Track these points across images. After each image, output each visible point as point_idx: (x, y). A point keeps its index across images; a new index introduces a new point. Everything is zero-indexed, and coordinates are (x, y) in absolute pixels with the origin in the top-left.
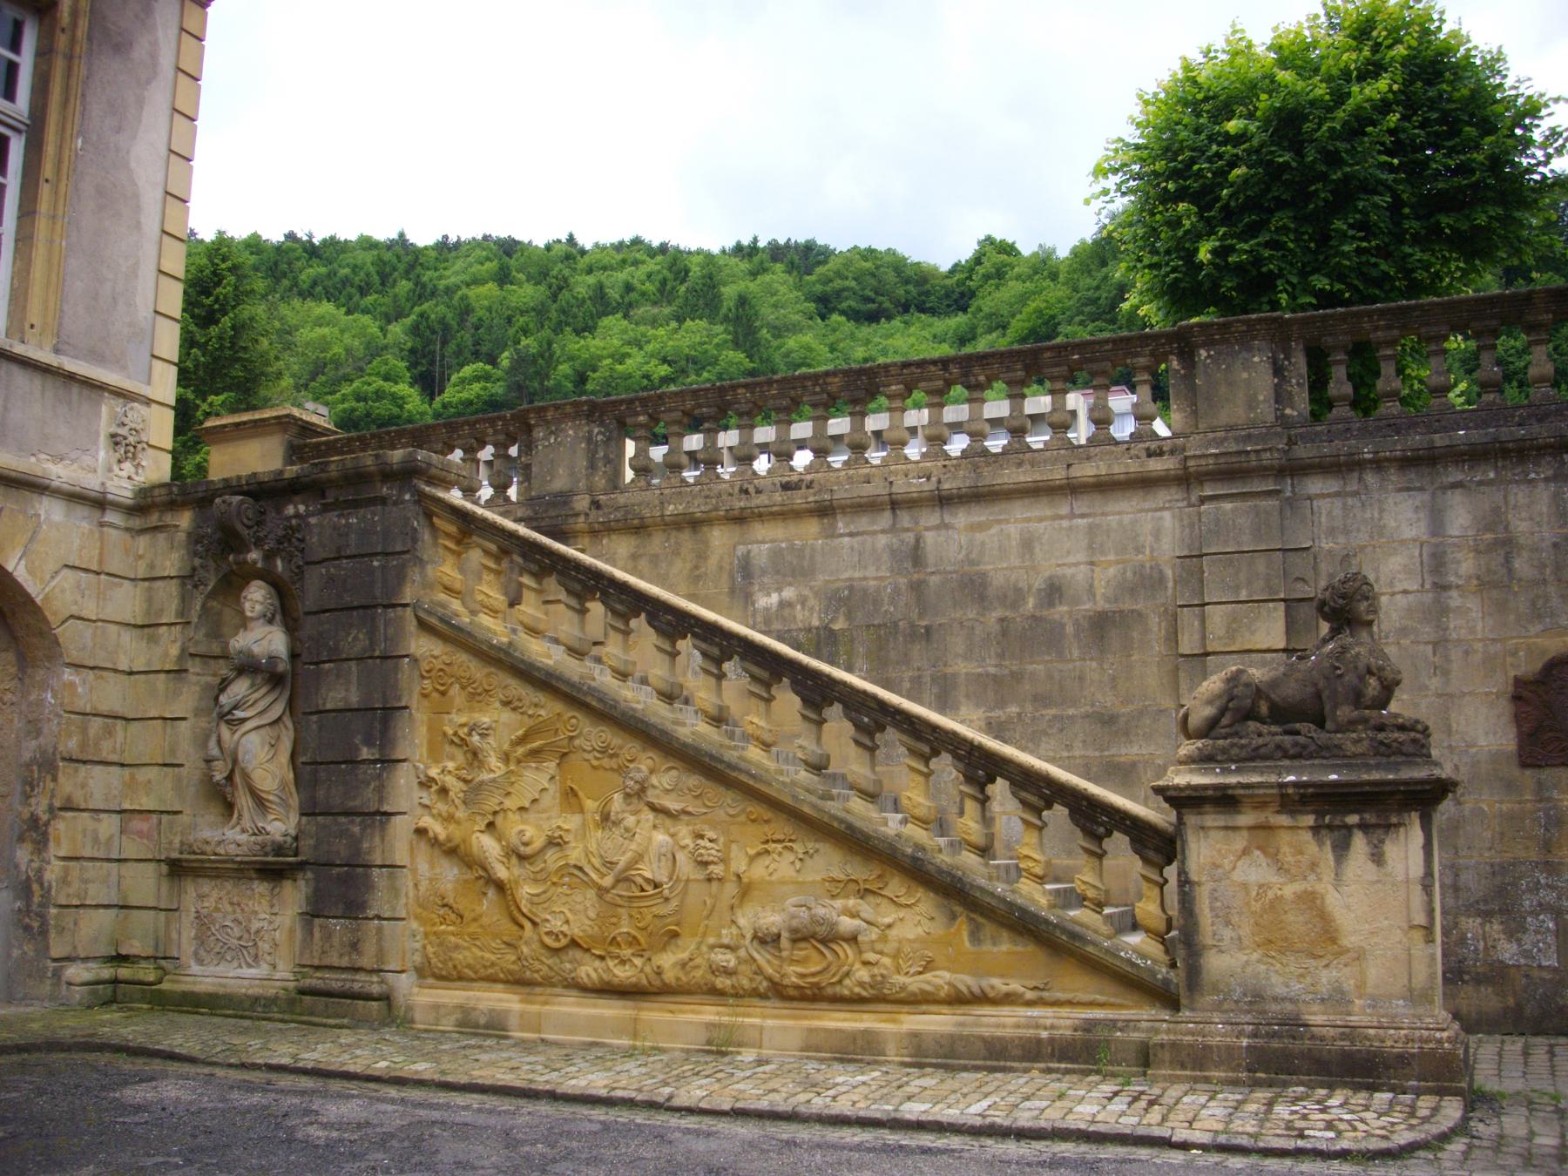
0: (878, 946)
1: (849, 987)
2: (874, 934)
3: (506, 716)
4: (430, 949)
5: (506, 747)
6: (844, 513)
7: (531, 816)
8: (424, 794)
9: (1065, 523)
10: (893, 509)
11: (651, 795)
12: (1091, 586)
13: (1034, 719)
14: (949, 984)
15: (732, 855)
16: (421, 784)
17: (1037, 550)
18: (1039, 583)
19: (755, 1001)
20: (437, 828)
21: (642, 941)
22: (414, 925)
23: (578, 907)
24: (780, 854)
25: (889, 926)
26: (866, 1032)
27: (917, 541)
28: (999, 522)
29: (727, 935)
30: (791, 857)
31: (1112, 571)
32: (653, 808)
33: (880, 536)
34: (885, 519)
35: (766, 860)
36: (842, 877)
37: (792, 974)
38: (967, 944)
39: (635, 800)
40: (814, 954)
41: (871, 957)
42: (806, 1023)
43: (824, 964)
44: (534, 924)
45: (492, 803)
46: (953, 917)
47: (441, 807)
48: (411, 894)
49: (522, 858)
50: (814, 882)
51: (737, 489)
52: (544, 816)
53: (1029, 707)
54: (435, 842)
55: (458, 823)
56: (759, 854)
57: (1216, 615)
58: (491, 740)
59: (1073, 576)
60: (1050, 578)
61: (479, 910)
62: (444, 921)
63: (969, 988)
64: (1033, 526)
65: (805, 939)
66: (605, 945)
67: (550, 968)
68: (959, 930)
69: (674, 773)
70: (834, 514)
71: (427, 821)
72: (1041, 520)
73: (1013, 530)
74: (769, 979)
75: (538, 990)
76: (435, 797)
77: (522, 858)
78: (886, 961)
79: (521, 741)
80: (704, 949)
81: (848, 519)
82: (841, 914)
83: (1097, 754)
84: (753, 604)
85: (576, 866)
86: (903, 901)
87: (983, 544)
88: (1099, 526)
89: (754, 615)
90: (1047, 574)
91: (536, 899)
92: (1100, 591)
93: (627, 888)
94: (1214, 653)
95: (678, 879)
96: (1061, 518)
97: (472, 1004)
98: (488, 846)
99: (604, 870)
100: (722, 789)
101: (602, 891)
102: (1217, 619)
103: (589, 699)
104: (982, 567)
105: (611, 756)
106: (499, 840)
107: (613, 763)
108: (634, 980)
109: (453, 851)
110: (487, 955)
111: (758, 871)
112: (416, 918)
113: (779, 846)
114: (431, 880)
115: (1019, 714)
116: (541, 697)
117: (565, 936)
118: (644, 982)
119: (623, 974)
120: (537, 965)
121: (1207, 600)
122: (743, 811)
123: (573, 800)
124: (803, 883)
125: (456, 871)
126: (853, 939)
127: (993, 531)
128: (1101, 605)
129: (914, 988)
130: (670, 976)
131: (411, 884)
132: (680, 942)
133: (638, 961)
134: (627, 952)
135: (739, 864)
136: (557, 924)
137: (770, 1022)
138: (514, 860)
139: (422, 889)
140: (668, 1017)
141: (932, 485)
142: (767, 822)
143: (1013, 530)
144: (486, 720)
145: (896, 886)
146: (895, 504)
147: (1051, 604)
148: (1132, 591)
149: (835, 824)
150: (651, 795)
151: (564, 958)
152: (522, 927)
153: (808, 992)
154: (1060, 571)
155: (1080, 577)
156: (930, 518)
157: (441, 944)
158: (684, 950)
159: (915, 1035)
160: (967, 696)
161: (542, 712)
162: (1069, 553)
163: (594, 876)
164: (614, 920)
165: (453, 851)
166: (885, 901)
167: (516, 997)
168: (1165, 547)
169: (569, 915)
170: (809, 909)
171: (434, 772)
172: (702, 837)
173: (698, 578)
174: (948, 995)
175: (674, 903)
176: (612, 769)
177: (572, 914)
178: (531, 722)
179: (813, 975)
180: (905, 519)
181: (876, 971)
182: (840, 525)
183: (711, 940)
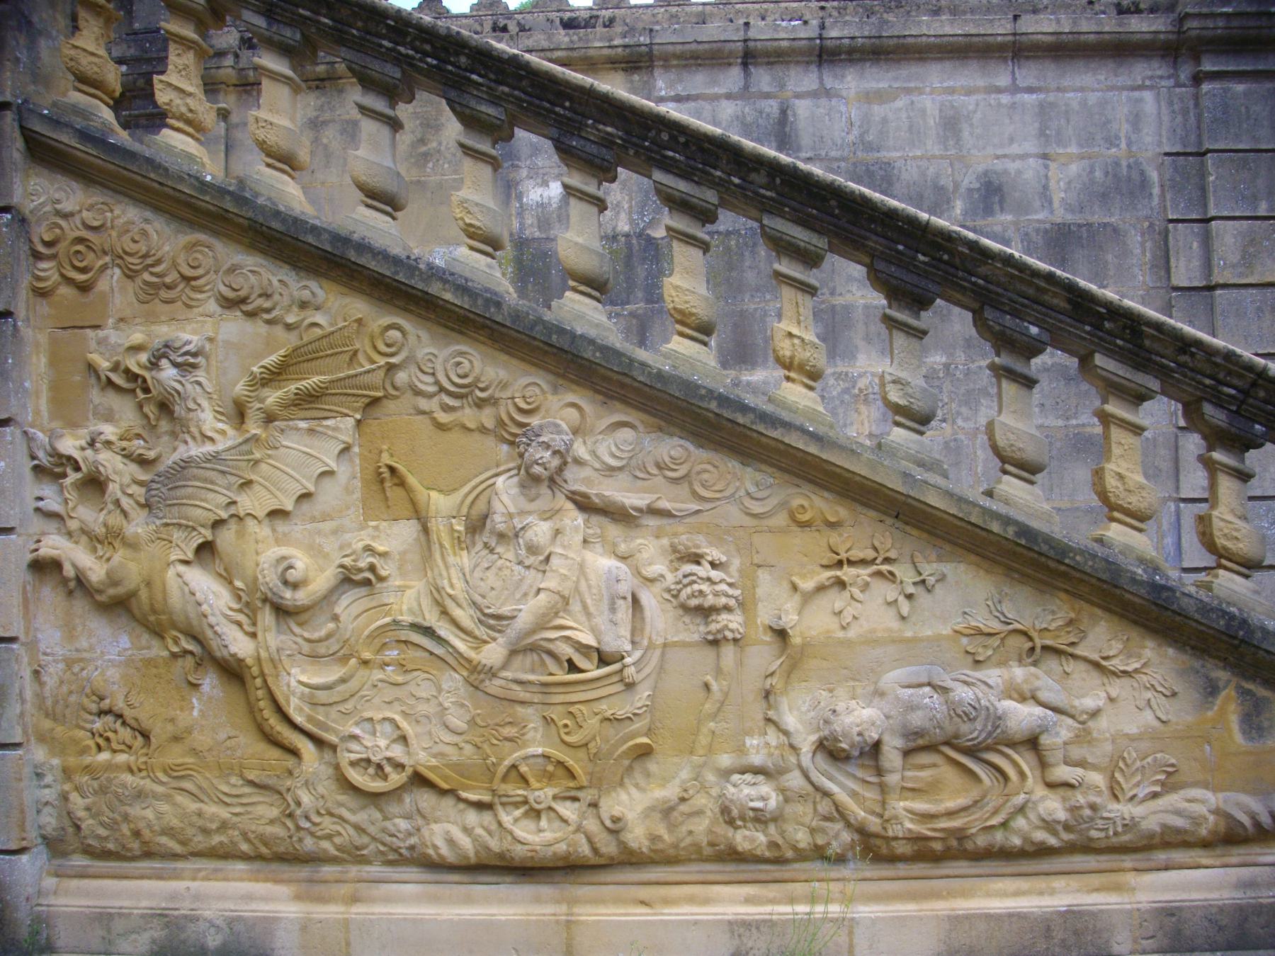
0: (1076, 753)
1: (1025, 829)
2: (1064, 730)
3: (233, 327)
4: (77, 801)
5: (240, 388)
6: (666, 67)
7: (297, 528)
8: (48, 490)
9: (1005, 99)
10: (745, 65)
11: (576, 479)
12: (1046, 187)
13: (968, 373)
14: (1217, 812)
15: (760, 592)
16: (38, 470)
17: (966, 134)
18: (969, 180)
19: (816, 867)
20: (78, 557)
21: (578, 770)
22: (39, 754)
23: (423, 708)
24: (865, 587)
25: (1095, 714)
26: (1071, 915)
27: (784, 112)
28: (908, 91)
29: (758, 749)
30: (891, 592)
31: (1074, 168)
32: (584, 504)
33: (724, 103)
34: (732, 78)
35: (837, 600)
36: (995, 626)
37: (905, 815)
38: (1238, 737)
39: (544, 490)
40: (948, 774)
41: (1063, 772)
42: (942, 907)
43: (975, 794)
44: (319, 742)
45: (213, 503)
46: (1212, 690)
47: (87, 514)
48: (28, 694)
49: (282, 612)
50: (938, 638)
51: (488, 26)
52: (327, 526)
53: (961, 357)
54: (80, 585)
55: (132, 545)
56: (821, 588)
57: (1228, 236)
58: (201, 376)
59: (1019, 172)
60: (986, 173)
61: (184, 719)
62: (102, 743)
63: (1253, 817)
64: (958, 99)
65: (931, 748)
66: (494, 785)
67: (359, 829)
68: (1223, 711)
69: (626, 434)
70: (651, 68)
71: (54, 545)
72: (969, 92)
73: (929, 104)
74: (862, 831)
75: (328, 870)
76: (72, 496)
77: (282, 612)
78: (1097, 778)
79: (274, 376)
80: (711, 777)
81: (672, 75)
82: (1006, 693)
83: (1060, 423)
84: (519, 197)
85: (415, 627)
86: (1116, 664)
87: (885, 121)
88: (1052, 105)
89: (520, 214)
90: (980, 168)
91: (322, 696)
92: (1058, 196)
93: (562, 665)
94: (1225, 286)
95: (651, 646)
96: (999, 90)
97: (185, 908)
98: (206, 591)
99: (481, 632)
100: (733, 465)
101: (477, 675)
102: (1229, 239)
103: (435, 289)
104: (885, 155)
105: (480, 404)
106: (227, 579)
107: (487, 417)
108: (562, 847)
109: (118, 605)
110: (211, 809)
111: (813, 623)
112: (42, 739)
113: (864, 572)
114: (69, 663)
115: (947, 366)
116: (316, 289)
117: (399, 766)
118: (585, 850)
119: (535, 837)
120: (328, 824)
121: (1212, 212)
122: (783, 504)
123: (394, 493)
124: (915, 640)
125: (125, 641)
126: (1032, 743)
127: (899, 103)
128: (1060, 215)
129: (1151, 824)
130: (637, 836)
131: (27, 674)
132: (652, 766)
133: (567, 810)
134: (543, 794)
135: (776, 604)
136: (381, 745)
137: (865, 911)
138: (267, 617)
139: (50, 681)
140: (640, 914)
141: (812, 31)
142: (832, 525)
143: (929, 104)
144: (189, 336)
145: (1102, 637)
146: (750, 57)
147: (988, 211)
148: (1104, 197)
149: (995, 527)
150: (576, 479)
151: (393, 809)
152: (294, 752)
153: (938, 846)
154: (999, 165)
155: (1029, 175)
156: (803, 80)
157: (103, 790)
158: (664, 782)
159: (1169, 912)
160: (868, 339)
161: (319, 318)
162: (1012, 140)
163: (461, 646)
164: (509, 731)
165: (118, 605)
166: (1082, 666)
167: (283, 890)
168: (1148, 139)
169: (404, 724)
170: (944, 690)
171: (69, 445)
172: (697, 559)
173: (426, 156)
174: (1214, 832)
175: (643, 695)
176: (483, 430)
177: (411, 720)
178: (292, 340)
179: (950, 814)
180: (763, 79)
181: (1080, 798)
182: (660, 83)
183: (725, 760)
